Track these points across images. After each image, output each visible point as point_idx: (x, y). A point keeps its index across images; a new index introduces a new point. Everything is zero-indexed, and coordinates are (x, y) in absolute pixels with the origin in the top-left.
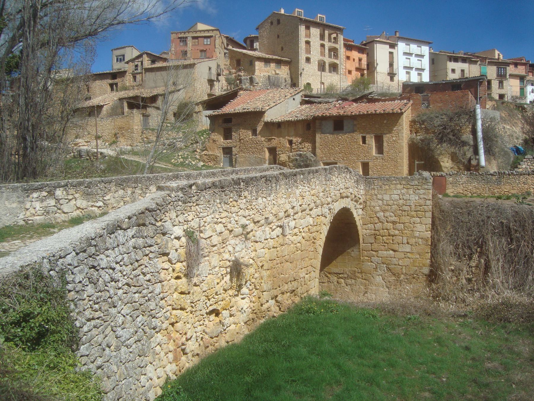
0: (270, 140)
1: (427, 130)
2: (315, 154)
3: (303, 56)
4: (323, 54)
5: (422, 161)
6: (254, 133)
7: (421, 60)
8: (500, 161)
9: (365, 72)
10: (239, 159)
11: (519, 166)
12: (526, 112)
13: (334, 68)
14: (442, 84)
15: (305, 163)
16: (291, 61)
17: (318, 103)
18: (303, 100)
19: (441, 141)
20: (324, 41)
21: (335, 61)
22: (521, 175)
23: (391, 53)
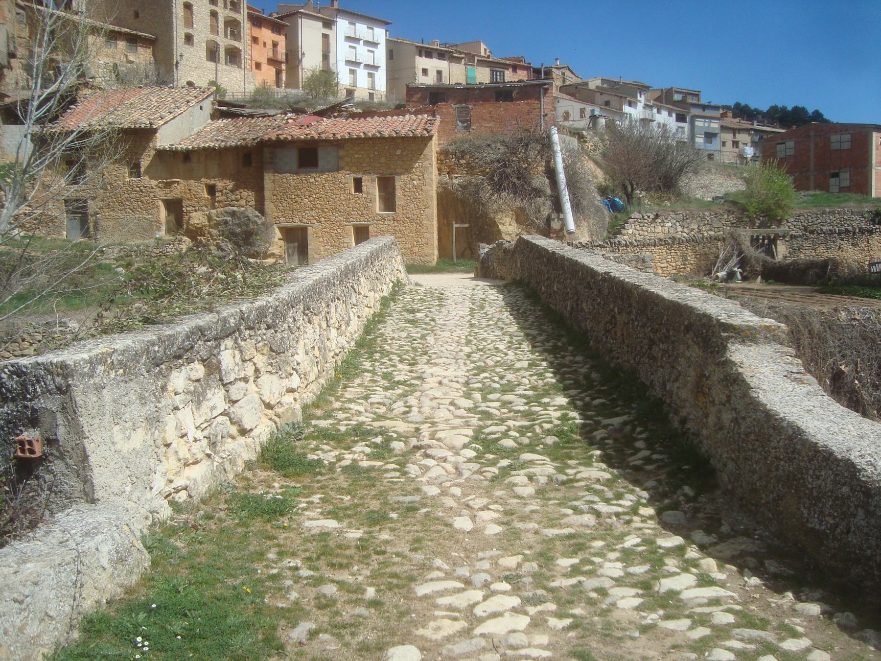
0: (168, 185)
1: (470, 169)
2: (262, 211)
3: (179, 31)
4: (214, 29)
5: (463, 222)
6: (135, 169)
7: (373, 52)
8: (591, 221)
9: (284, 67)
10: (103, 223)
11: (623, 231)
12: (586, 142)
13: (233, 56)
14: (479, 89)
15: (244, 228)
16: (156, 39)
17: (248, 117)
18: (216, 109)
19: (498, 188)
20: (216, 5)
21: (236, 44)
22: (644, 246)
23: (325, 37)
